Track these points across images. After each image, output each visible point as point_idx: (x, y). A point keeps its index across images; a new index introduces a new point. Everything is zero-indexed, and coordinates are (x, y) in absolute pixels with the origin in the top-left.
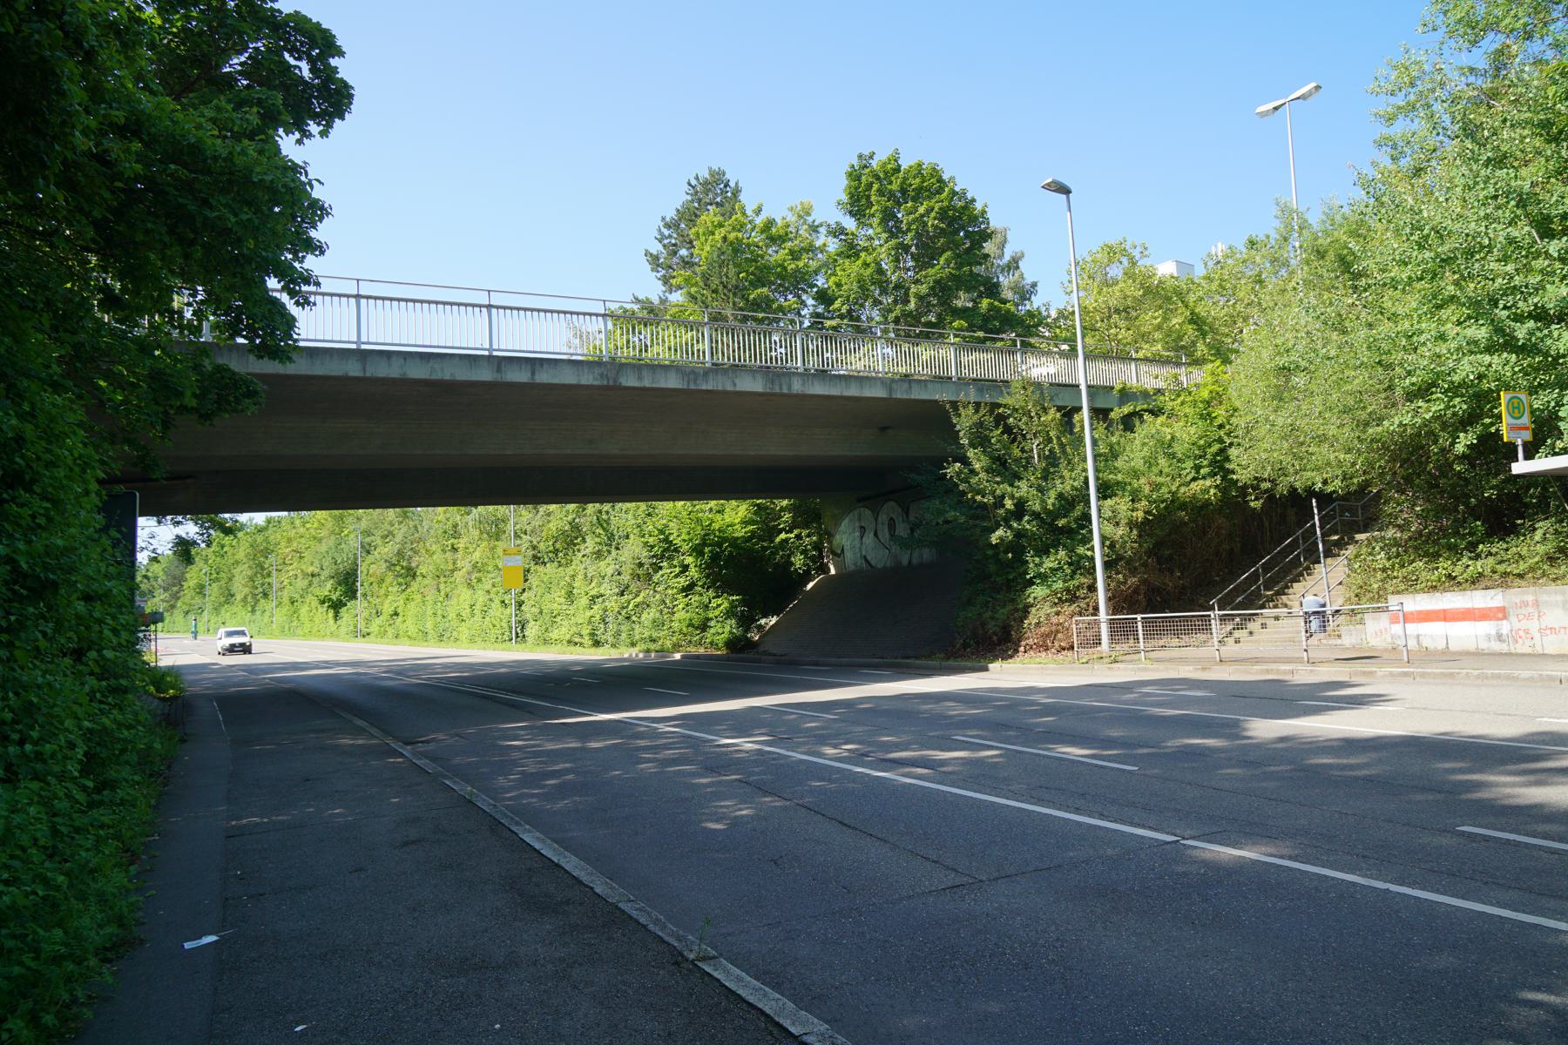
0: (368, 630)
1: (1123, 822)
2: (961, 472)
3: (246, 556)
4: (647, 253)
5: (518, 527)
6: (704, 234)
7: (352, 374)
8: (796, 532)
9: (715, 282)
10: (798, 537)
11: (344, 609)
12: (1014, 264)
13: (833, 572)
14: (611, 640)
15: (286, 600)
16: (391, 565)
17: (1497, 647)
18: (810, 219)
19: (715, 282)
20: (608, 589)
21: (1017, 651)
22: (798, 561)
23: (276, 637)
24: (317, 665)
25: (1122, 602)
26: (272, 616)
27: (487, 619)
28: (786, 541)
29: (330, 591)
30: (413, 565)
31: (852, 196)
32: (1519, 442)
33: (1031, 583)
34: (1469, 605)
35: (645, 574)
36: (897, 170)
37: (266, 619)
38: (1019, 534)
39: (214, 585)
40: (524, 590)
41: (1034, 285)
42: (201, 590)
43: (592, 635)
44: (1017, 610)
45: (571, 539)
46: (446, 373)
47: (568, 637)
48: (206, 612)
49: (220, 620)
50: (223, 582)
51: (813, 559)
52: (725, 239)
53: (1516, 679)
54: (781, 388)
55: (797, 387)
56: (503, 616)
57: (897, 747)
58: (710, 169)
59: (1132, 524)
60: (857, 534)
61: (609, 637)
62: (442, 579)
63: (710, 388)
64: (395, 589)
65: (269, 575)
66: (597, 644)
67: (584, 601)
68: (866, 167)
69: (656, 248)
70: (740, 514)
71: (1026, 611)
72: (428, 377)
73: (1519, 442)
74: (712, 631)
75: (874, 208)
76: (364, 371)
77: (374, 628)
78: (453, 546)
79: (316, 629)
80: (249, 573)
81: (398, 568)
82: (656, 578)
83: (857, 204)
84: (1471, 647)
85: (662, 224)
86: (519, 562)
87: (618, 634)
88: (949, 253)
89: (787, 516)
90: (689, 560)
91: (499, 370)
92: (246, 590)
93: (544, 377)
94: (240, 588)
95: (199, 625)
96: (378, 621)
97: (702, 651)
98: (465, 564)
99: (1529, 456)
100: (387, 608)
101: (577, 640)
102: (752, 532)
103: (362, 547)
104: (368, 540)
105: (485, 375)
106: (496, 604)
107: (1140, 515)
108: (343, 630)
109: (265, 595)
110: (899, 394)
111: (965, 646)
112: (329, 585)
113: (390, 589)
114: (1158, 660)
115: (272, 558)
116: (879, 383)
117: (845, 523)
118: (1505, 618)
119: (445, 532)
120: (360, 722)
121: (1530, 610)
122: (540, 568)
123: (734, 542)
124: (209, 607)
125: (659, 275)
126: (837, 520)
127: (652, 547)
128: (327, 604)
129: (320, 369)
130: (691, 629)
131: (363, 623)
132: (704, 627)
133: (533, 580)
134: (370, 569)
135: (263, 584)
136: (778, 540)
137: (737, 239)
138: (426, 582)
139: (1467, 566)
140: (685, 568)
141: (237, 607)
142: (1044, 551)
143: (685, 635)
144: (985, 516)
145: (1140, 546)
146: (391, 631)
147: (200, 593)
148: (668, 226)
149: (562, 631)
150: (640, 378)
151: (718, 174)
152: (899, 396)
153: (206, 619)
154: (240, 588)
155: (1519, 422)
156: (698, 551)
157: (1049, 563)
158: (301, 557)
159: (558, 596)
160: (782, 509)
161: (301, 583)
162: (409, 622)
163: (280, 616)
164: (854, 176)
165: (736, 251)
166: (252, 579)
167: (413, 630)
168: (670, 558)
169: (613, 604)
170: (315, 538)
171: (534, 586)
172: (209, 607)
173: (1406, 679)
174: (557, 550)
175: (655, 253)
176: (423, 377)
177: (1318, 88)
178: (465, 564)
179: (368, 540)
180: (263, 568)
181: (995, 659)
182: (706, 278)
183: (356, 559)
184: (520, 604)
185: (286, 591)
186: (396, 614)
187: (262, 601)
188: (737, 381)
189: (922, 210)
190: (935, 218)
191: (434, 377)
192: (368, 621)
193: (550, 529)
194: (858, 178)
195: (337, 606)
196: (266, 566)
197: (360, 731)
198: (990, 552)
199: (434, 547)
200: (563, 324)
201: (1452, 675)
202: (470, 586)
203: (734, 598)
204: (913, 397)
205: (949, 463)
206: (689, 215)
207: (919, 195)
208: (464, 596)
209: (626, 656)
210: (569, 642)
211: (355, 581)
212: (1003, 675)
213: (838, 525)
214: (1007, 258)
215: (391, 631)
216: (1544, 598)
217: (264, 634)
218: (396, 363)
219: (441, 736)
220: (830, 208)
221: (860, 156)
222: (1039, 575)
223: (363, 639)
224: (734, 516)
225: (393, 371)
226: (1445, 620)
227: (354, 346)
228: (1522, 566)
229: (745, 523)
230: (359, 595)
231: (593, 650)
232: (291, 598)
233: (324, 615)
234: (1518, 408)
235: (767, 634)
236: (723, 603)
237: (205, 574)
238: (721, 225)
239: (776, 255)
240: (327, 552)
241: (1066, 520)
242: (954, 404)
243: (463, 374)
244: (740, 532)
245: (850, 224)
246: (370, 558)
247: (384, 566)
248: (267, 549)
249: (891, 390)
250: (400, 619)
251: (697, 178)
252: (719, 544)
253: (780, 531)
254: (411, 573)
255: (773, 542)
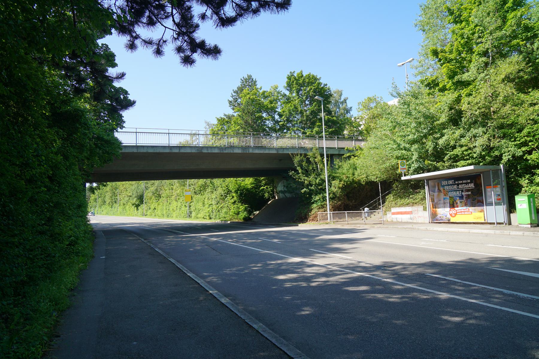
4: (228, 100)
5: (190, 183)
6: (244, 96)
7: (134, 152)
8: (266, 186)
10: (267, 188)
12: (345, 101)
13: (277, 198)
15: (122, 204)
16: (154, 194)
17: (411, 221)
18: (278, 90)
20: (214, 202)
21: (307, 221)
22: (266, 195)
24: (129, 224)
25: (335, 208)
26: (118, 209)
27: (181, 211)
28: (264, 189)
30: (160, 193)
31: (288, 84)
33: (313, 203)
35: (223, 198)
36: (302, 76)
37: (116, 210)
38: (310, 190)
41: (351, 108)
42: (95, 200)
43: (209, 216)
44: (309, 210)
45: (204, 187)
46: (158, 151)
49: (102, 210)
51: (271, 194)
52: (249, 98)
53: (397, 228)
54: (246, 151)
55: (251, 151)
56: (185, 210)
57: (197, 229)
58: (248, 75)
59: (339, 188)
60: (283, 187)
61: (213, 217)
63: (226, 152)
66: (210, 218)
67: (207, 206)
68: (292, 75)
69: (231, 99)
72: (153, 152)
73: (403, 172)
74: (240, 215)
76: (138, 151)
77: (148, 213)
80: (110, 195)
81: (156, 194)
82: (226, 199)
83: (289, 86)
84: (406, 221)
87: (216, 215)
88: (316, 103)
89: (264, 182)
90: (234, 195)
92: (110, 201)
93: (182, 151)
94: (108, 200)
96: (150, 211)
99: (405, 175)
100: (152, 207)
101: (205, 217)
103: (145, 187)
104: (147, 185)
105: (167, 151)
106: (183, 206)
107: (341, 185)
108: (139, 213)
109: (116, 202)
110: (280, 152)
112: (135, 199)
113: (153, 201)
115: (118, 190)
116: (274, 149)
118: (412, 214)
119: (170, 184)
120: (135, 235)
121: (416, 212)
123: (247, 189)
124: (98, 206)
125: (231, 108)
126: (278, 183)
127: (225, 190)
128: (134, 206)
129: (127, 151)
130: (234, 214)
131: (145, 212)
132: (238, 214)
133: (194, 199)
134: (148, 194)
136: (260, 189)
137: (253, 98)
138: (164, 199)
140: (233, 197)
141: (107, 206)
142: (316, 195)
143: (233, 216)
144: (302, 185)
147: (95, 201)
148: (235, 92)
150: (208, 150)
152: (280, 153)
154: (108, 200)
155: (403, 167)
156: (236, 192)
157: (317, 198)
158: (127, 191)
159: (200, 204)
160: (262, 180)
163: (120, 209)
164: (289, 78)
165: (253, 101)
166: (111, 197)
167: (160, 214)
168: (230, 194)
169: (214, 207)
170: (131, 184)
171: (194, 201)
172: (98, 206)
177: (413, 59)
179: (147, 185)
180: (115, 194)
181: (300, 224)
182: (243, 110)
183: (143, 191)
184: (190, 206)
185: (122, 201)
186: (155, 209)
187: (115, 204)
188: (234, 150)
189: (308, 89)
190: (312, 92)
191: (155, 152)
192: (147, 211)
193: (198, 184)
195: (137, 206)
196: (116, 193)
197: (134, 237)
199: (167, 188)
200: (189, 137)
201: (388, 227)
202: (176, 201)
205: (290, 171)
206: (241, 89)
207: (310, 83)
208: (174, 204)
209: (217, 222)
210: (203, 218)
211: (143, 198)
212: (302, 227)
213: (278, 184)
216: (419, 209)
218: (145, 148)
219: (153, 238)
221: (291, 72)
222: (315, 201)
224: (248, 182)
225: (144, 151)
226: (401, 214)
227: (135, 145)
228: (417, 201)
230: (144, 202)
231: (210, 220)
232: (123, 203)
233: (133, 208)
234: (403, 164)
235: (255, 216)
236: (242, 208)
237: (97, 195)
238: (249, 94)
239: (266, 102)
241: (321, 187)
242: (292, 154)
243: (162, 151)
244: (250, 187)
245: (287, 93)
246: (147, 191)
248: (116, 187)
249: (278, 151)
251: (243, 78)
252: (243, 190)
253: (262, 186)
255: (259, 189)
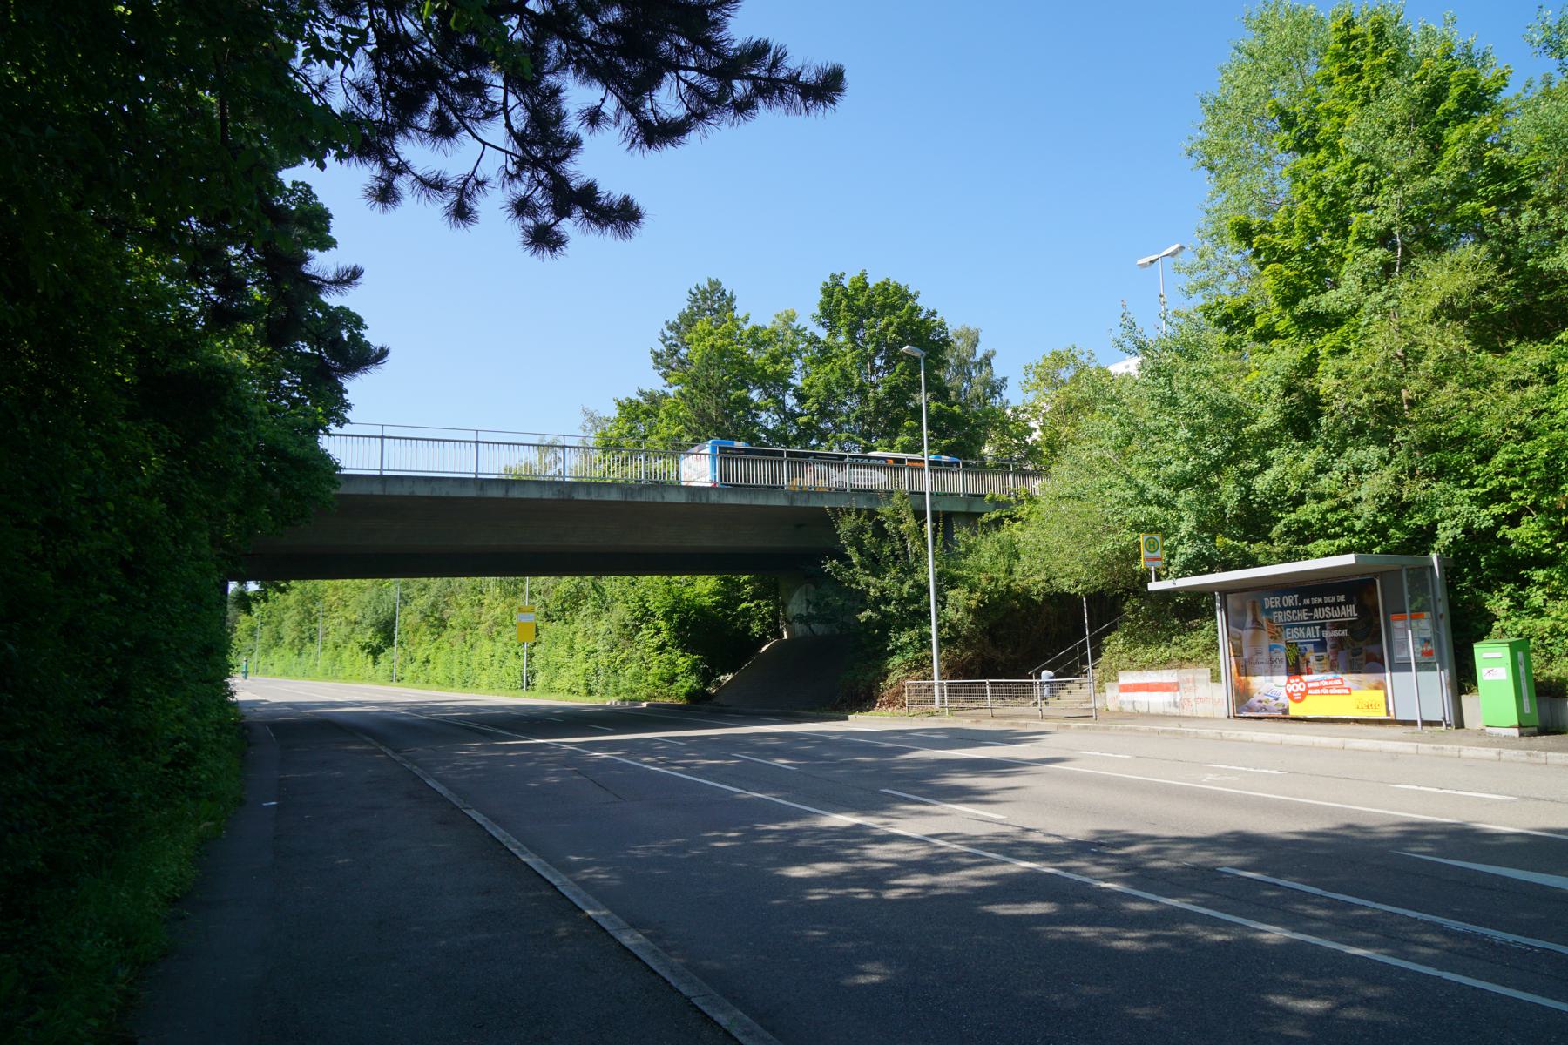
0: (403, 676)
1: (725, 783)
2: (837, 566)
3: (296, 602)
4: (652, 351)
5: (534, 587)
8: (755, 602)
9: (702, 383)
10: (758, 606)
11: (383, 654)
12: (987, 360)
13: (786, 637)
14: (600, 689)
15: (330, 645)
16: (425, 617)
17: (1175, 711)
19: (702, 383)
21: (874, 706)
22: (756, 627)
23: (320, 680)
24: (360, 704)
25: (955, 670)
26: (317, 659)
27: (504, 668)
28: (748, 609)
29: (370, 638)
30: (445, 616)
31: (824, 310)
32: (1153, 569)
33: (892, 653)
34: (1160, 681)
35: (629, 633)
37: (311, 662)
39: (264, 628)
40: (535, 643)
41: (1004, 380)
43: (587, 685)
44: (880, 674)
45: (574, 601)
46: (443, 492)
47: (568, 687)
48: (256, 654)
49: (269, 661)
50: (273, 625)
52: (713, 346)
53: (1136, 730)
54: (700, 499)
56: (517, 665)
58: (709, 279)
59: (968, 610)
60: (804, 605)
62: (468, 631)
63: (643, 500)
64: (428, 638)
65: (316, 620)
66: (590, 693)
67: (581, 656)
68: (837, 284)
69: (660, 347)
70: (709, 586)
71: (886, 674)
73: (1153, 569)
74: (678, 684)
75: (843, 322)
77: (408, 674)
78: (479, 600)
79: (356, 673)
80: (297, 618)
81: (432, 619)
82: (637, 638)
83: (829, 314)
85: (665, 327)
86: (531, 619)
87: (607, 684)
89: (749, 589)
90: (662, 624)
91: (482, 488)
92: (294, 634)
93: (515, 493)
94: (289, 634)
95: (250, 665)
96: (412, 667)
97: (668, 700)
98: (487, 618)
99: (1158, 578)
100: (420, 656)
102: (717, 602)
103: (401, 598)
104: (407, 591)
105: (471, 492)
106: (511, 656)
107: (973, 603)
108: (381, 674)
109: (312, 639)
111: (843, 701)
112: (370, 632)
113: (424, 638)
114: (957, 715)
117: (795, 596)
118: (1178, 690)
119: (474, 588)
120: (367, 739)
122: (548, 626)
123: (701, 610)
124: (259, 648)
125: (661, 372)
128: (366, 650)
132: (672, 680)
133: (544, 636)
134: (407, 619)
135: (310, 629)
138: (455, 632)
139: (1164, 652)
140: (658, 631)
141: (285, 650)
144: (861, 599)
145: (977, 626)
146: (422, 677)
147: (251, 635)
148: (670, 328)
149: (562, 682)
150: (589, 493)
151: (715, 284)
153: (256, 660)
154: (289, 634)
156: (668, 616)
158: (346, 606)
159: (562, 650)
160: (745, 582)
161: (345, 630)
162: (438, 670)
164: (828, 292)
165: (722, 355)
166: (299, 624)
167: (441, 677)
168: (648, 622)
169: (603, 659)
172: (259, 648)
173: (1086, 731)
174: (565, 609)
175: (659, 351)
176: (426, 494)
177: (1182, 248)
178: (487, 618)
179: (407, 591)
180: (310, 614)
182: (695, 379)
183: (395, 609)
184: (531, 656)
185: (330, 637)
187: (309, 645)
188: (665, 495)
191: (434, 494)
192: (403, 667)
193: (558, 591)
194: (831, 296)
195: (375, 652)
196: (314, 612)
198: (862, 628)
201: (1108, 729)
202: (491, 638)
203: (696, 657)
204: (810, 505)
208: (486, 646)
209: (608, 703)
210: (569, 690)
211: (394, 629)
212: (859, 723)
214: (979, 356)
215: (422, 677)
217: (309, 676)
220: (808, 319)
221: (833, 276)
222: (897, 648)
223: (397, 684)
224: (703, 588)
225: (404, 491)
227: (378, 473)
228: (1193, 652)
229: (714, 593)
230: (396, 641)
233: (364, 659)
236: (684, 663)
238: (711, 333)
239: (760, 358)
240: (369, 602)
241: (916, 606)
243: (455, 492)
245: (823, 334)
246: (408, 609)
247: (419, 617)
248: (315, 596)
250: (430, 666)
251: (697, 288)
252: (687, 612)
254: (442, 624)
255: (735, 610)
